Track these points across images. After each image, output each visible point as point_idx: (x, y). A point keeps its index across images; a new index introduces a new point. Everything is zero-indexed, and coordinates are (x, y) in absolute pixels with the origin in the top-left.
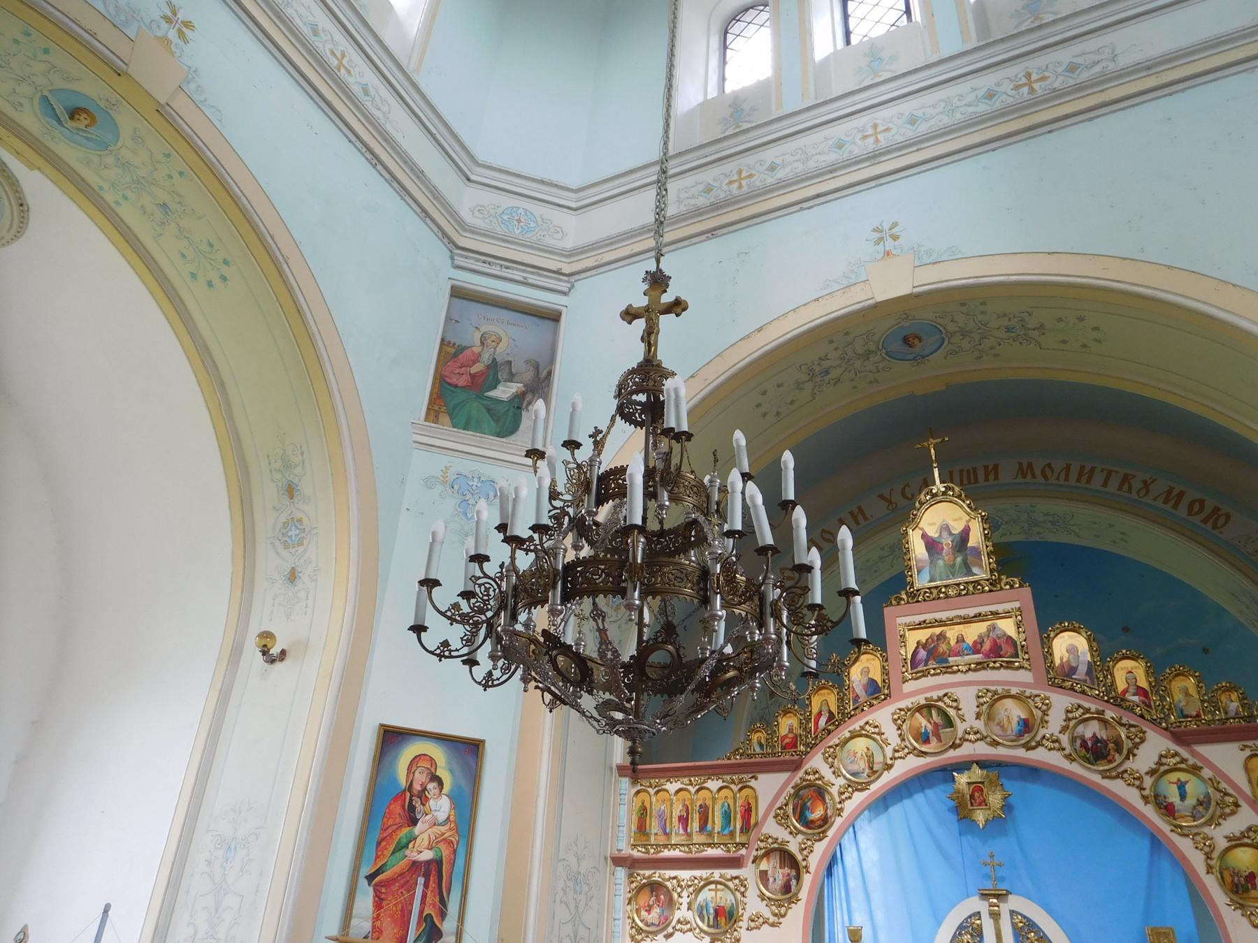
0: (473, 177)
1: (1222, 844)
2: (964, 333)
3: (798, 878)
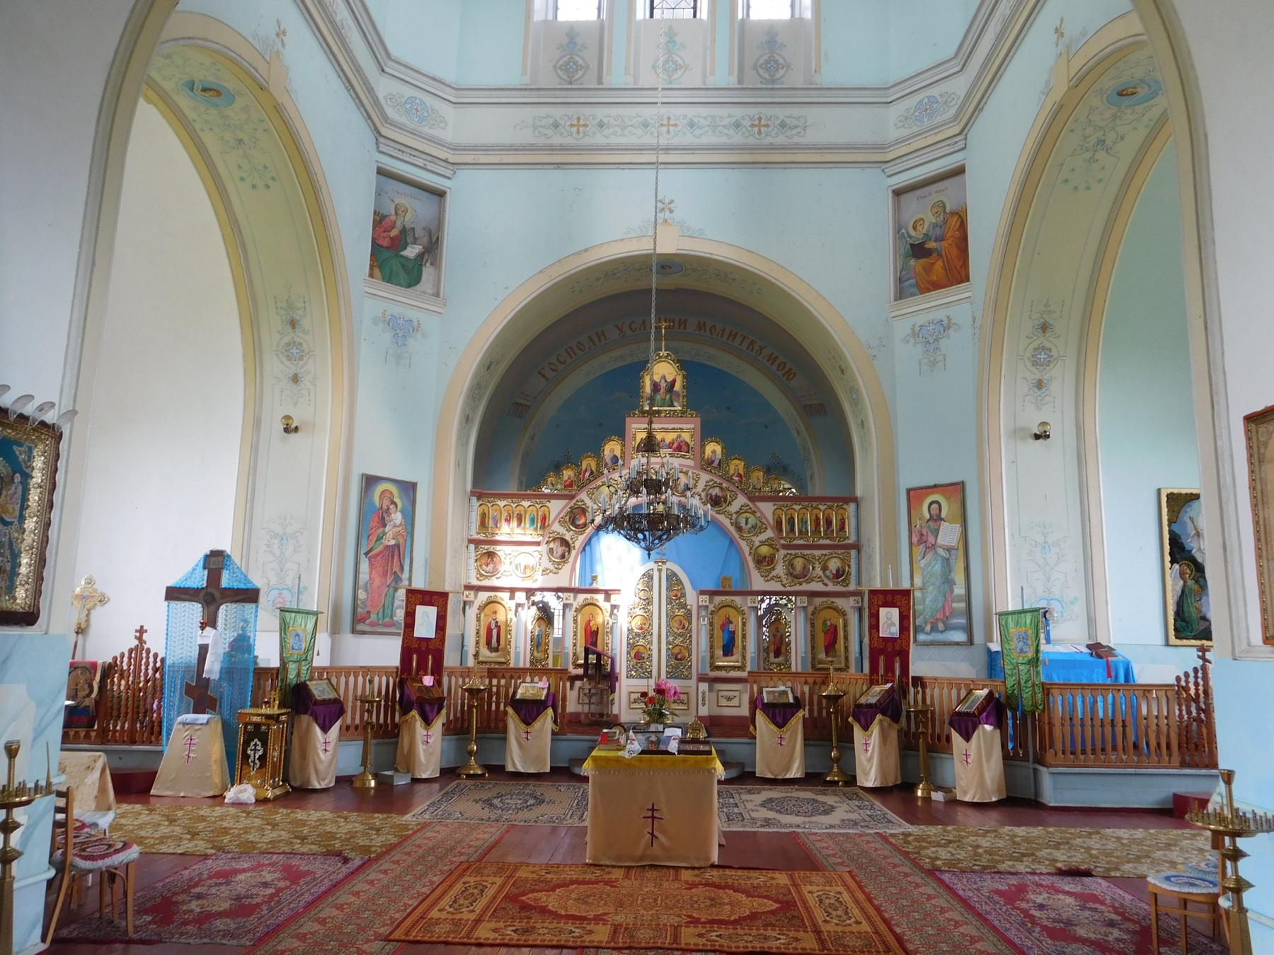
0: (387, 69)
1: (757, 544)
2: (694, 270)
3: (569, 552)
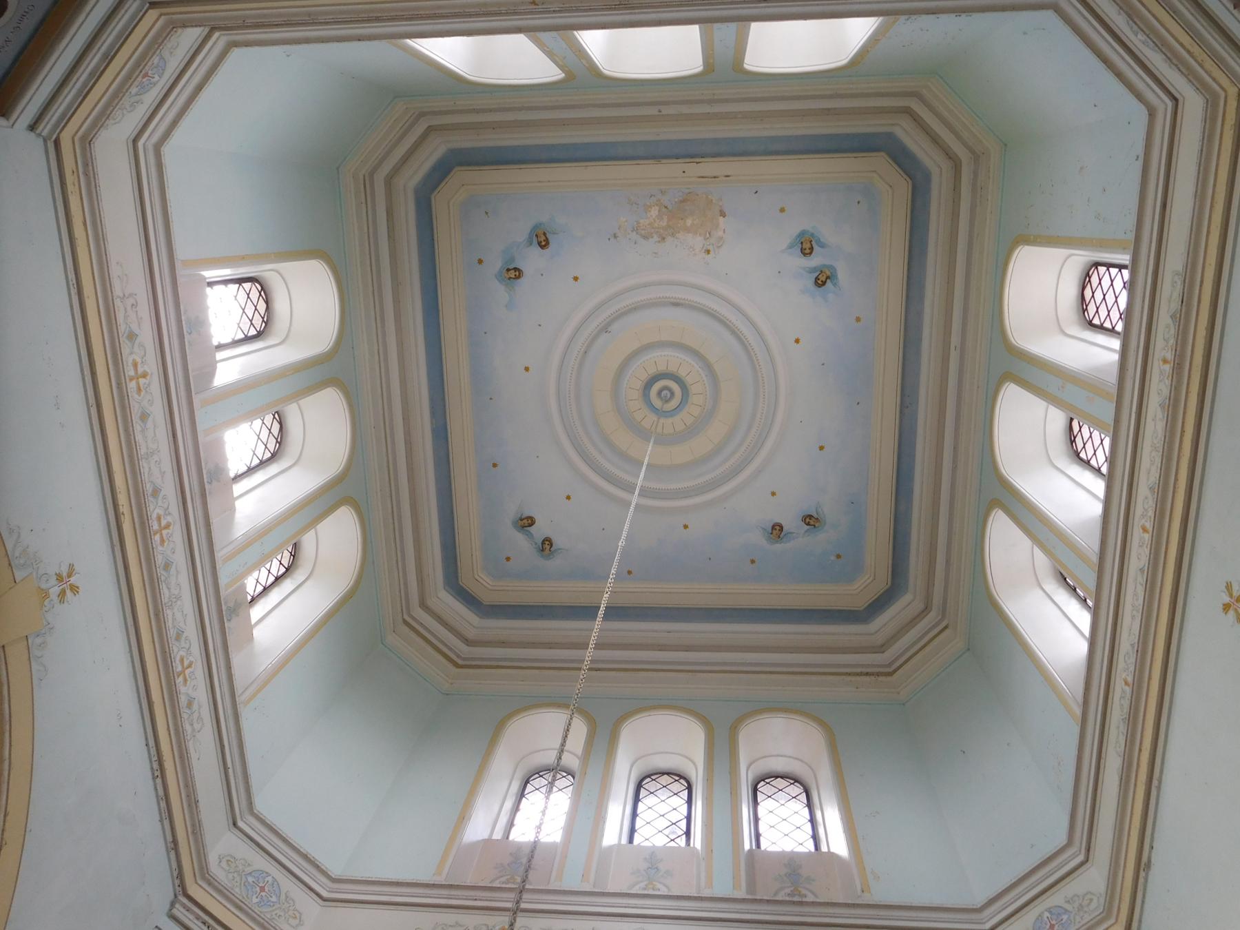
0: (240, 824)
